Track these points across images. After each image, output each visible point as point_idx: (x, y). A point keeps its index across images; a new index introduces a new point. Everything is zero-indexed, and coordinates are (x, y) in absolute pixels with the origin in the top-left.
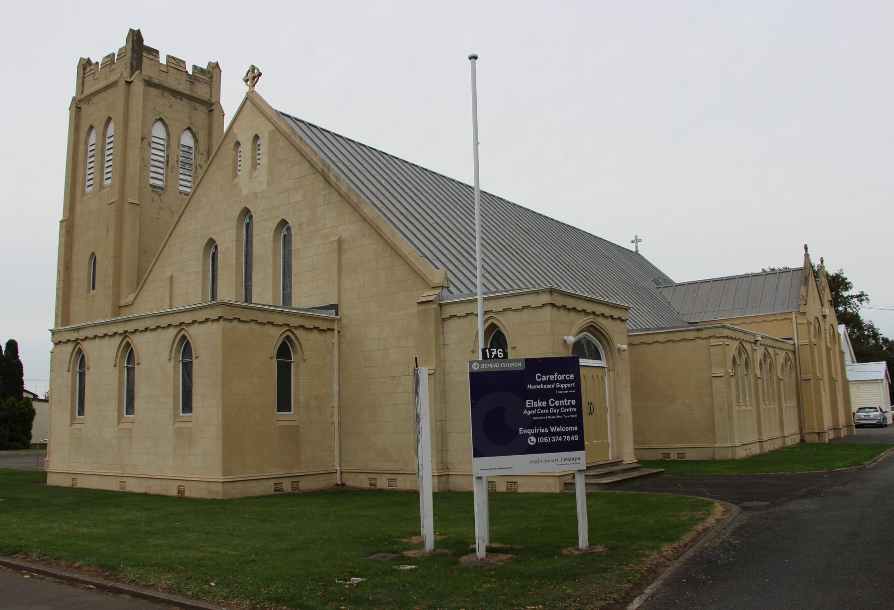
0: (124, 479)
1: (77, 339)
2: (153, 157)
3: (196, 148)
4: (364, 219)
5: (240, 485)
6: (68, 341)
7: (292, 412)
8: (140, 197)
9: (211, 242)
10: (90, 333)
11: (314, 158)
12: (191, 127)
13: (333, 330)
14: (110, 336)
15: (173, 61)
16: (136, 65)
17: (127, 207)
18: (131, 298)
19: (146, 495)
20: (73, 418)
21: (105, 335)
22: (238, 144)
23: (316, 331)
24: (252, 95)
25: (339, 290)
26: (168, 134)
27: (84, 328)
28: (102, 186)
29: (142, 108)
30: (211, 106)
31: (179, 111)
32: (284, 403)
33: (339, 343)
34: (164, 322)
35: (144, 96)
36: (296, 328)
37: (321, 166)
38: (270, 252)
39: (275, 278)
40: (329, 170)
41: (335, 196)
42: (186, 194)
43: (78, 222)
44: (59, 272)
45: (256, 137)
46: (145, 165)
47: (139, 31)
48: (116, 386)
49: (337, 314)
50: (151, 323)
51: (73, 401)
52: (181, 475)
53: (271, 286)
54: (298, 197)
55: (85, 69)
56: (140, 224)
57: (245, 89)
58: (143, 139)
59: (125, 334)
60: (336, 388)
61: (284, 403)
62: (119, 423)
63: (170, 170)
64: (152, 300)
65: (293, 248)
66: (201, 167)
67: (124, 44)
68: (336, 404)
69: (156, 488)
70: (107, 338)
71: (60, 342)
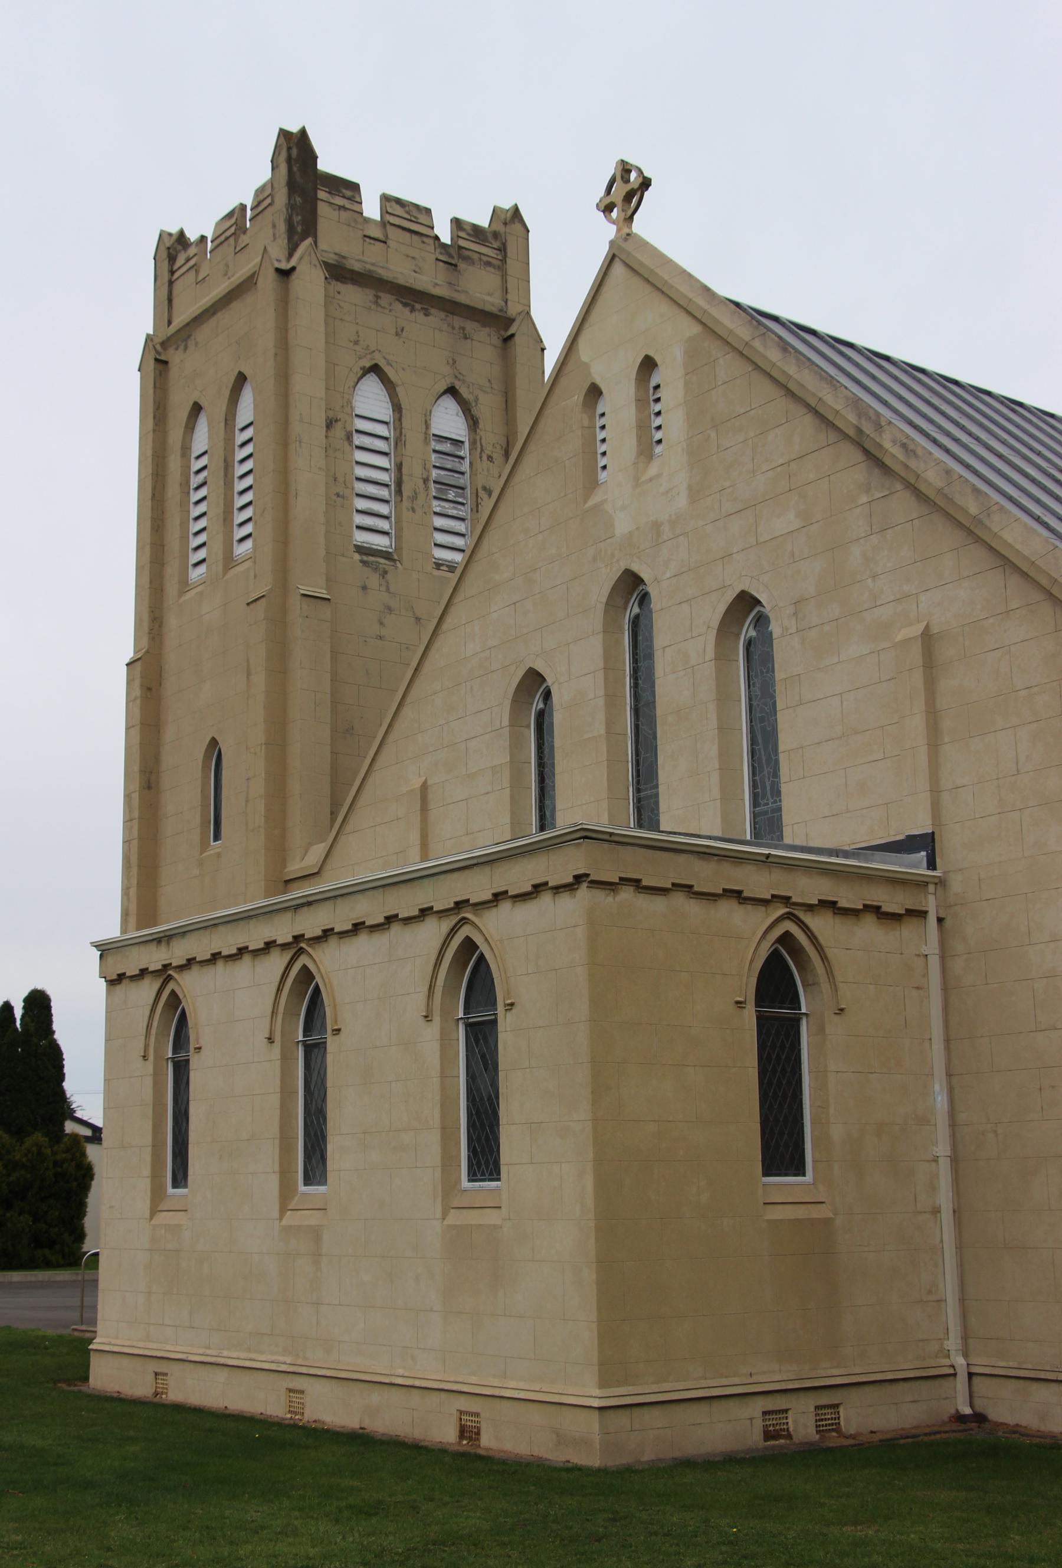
0: (298, 1383)
1: (166, 967)
2: (361, 472)
3: (473, 443)
4: (1005, 562)
5: (654, 1418)
6: (144, 972)
7: (809, 1177)
8: (329, 581)
9: (533, 680)
10: (200, 947)
11: (829, 399)
12: (458, 385)
13: (922, 914)
14: (256, 953)
15: (399, 210)
16: (302, 225)
17: (297, 608)
18: (318, 851)
19: (359, 1441)
20: (157, 1195)
21: (242, 951)
22: (595, 392)
23: (870, 919)
24: (628, 246)
25: (935, 791)
26: (397, 408)
27: (182, 933)
28: (229, 561)
29: (325, 331)
30: (506, 326)
31: (422, 346)
32: (782, 1150)
33: (944, 956)
34: (406, 903)
35: (326, 305)
36: (810, 908)
37: (852, 418)
38: (707, 691)
39: (727, 770)
40: (879, 427)
41: (903, 505)
42: (451, 568)
43: (173, 660)
44: (128, 797)
45: (648, 365)
46: (339, 494)
47: (303, 132)
48: (275, 1100)
49: (932, 864)
50: (370, 910)
51: (157, 1146)
52: (469, 1379)
53: (716, 792)
54: (784, 522)
55: (172, 259)
56: (335, 654)
57: (606, 231)
58: (330, 424)
59: (297, 945)
60: (941, 1101)
61: (782, 1150)
62: (283, 1209)
63: (406, 504)
64: (375, 847)
65: (779, 675)
66: (490, 493)
67: (264, 174)
68: (942, 1149)
69: (391, 1417)
70: (247, 958)
71: (121, 977)
